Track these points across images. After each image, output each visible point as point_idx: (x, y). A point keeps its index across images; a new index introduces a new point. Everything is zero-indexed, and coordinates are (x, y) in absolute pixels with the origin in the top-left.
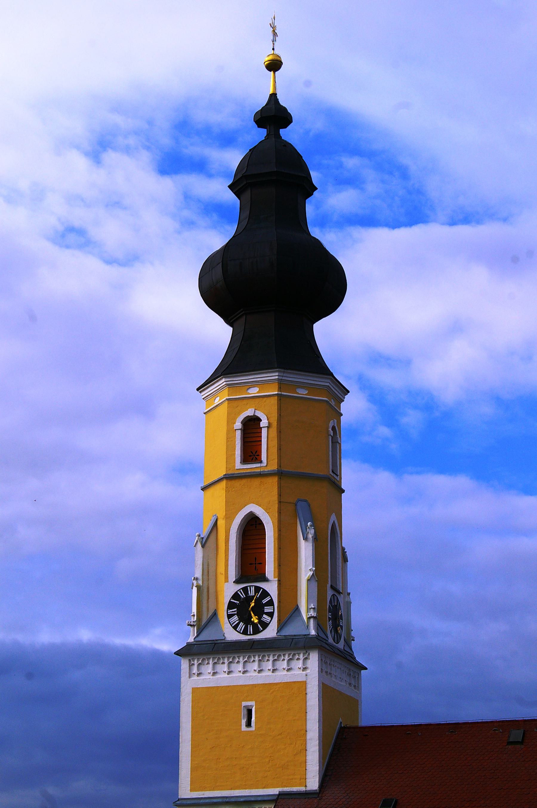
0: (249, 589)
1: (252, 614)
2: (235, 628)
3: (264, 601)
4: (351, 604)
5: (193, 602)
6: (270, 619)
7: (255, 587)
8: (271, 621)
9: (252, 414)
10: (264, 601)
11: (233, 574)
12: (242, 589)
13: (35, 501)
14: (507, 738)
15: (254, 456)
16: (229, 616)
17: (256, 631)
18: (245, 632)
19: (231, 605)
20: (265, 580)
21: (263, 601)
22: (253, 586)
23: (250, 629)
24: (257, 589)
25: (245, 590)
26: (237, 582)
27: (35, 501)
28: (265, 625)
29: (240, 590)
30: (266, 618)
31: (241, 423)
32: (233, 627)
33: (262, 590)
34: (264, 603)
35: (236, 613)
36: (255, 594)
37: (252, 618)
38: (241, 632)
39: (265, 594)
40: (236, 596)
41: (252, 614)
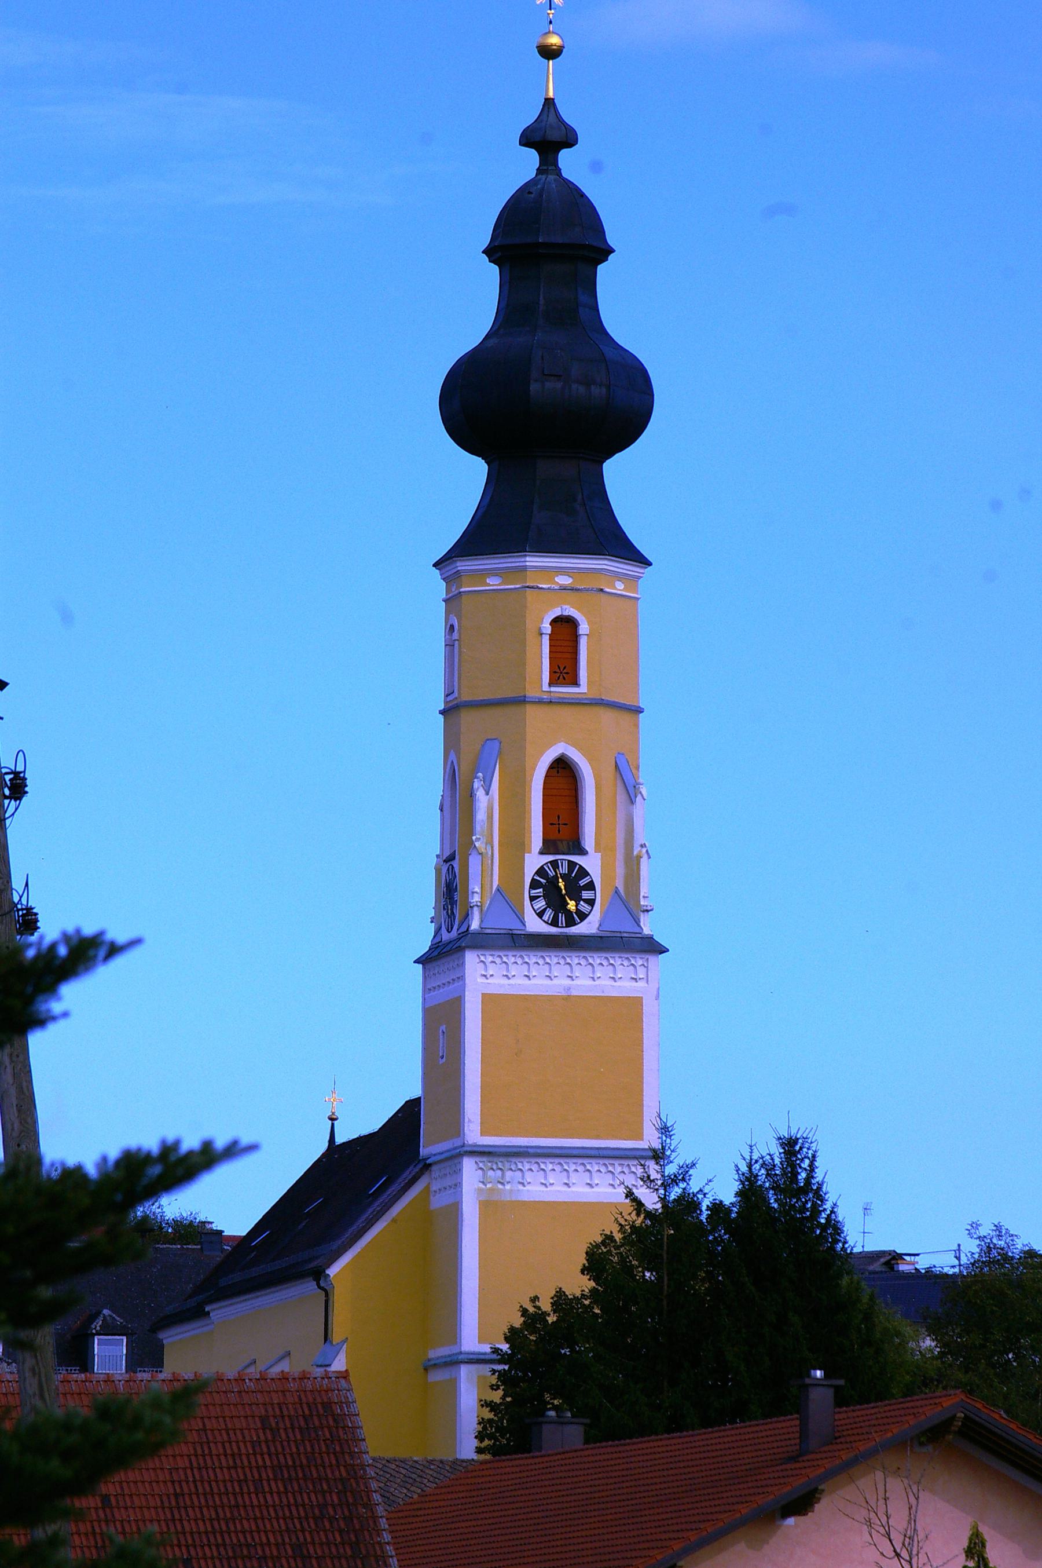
0: (560, 864)
1: (567, 899)
2: (540, 915)
3: (582, 883)
4: (434, 906)
5: (641, 878)
6: (590, 909)
7: (569, 861)
8: (591, 910)
9: (560, 614)
10: (582, 883)
11: (537, 841)
12: (551, 862)
13: (389, 724)
14: (16, 1396)
15: (561, 673)
16: (532, 899)
17: (571, 922)
18: (554, 923)
19: (534, 885)
20: (583, 852)
21: (580, 882)
22: (565, 860)
23: (562, 918)
24: (572, 865)
25: (554, 864)
26: (541, 853)
27: (389, 724)
28: (583, 916)
29: (547, 863)
30: (584, 907)
31: (550, 624)
32: (538, 914)
33: (578, 866)
34: (582, 885)
35: (542, 894)
36: (556, 872)
37: (568, 904)
38: (564, 925)
39: (583, 873)
40: (541, 872)
41: (567, 899)
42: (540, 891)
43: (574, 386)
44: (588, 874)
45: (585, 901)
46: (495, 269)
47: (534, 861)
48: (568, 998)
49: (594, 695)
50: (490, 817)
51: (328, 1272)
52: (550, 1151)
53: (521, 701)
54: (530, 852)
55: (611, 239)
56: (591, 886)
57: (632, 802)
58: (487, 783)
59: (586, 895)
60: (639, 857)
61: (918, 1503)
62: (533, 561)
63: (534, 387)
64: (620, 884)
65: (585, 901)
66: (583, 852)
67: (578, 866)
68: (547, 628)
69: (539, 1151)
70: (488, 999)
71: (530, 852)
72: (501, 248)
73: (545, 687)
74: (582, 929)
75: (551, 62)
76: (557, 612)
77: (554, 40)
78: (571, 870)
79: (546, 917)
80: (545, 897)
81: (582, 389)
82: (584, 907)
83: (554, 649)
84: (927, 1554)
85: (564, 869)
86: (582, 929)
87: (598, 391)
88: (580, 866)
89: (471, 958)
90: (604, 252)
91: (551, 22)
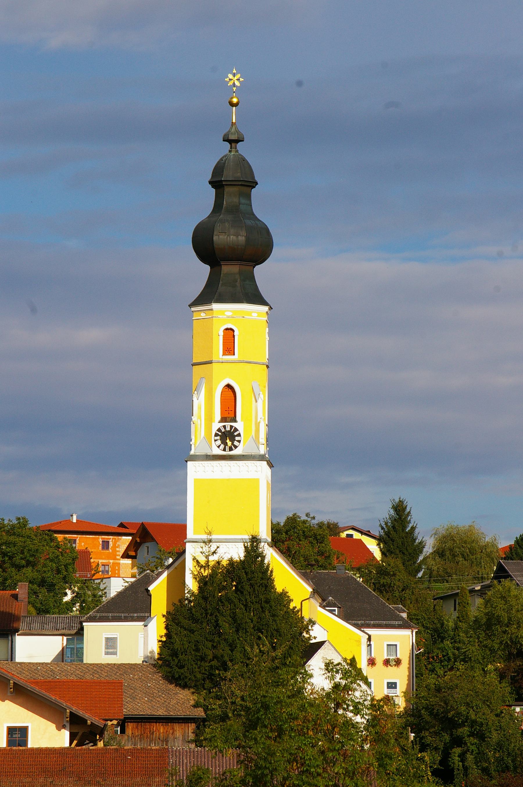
2: (219, 447)
3: (236, 434)
10: (236, 434)
11: (218, 416)
17: (231, 449)
18: (224, 450)
19: (216, 435)
20: (235, 421)
24: (231, 427)
25: (224, 427)
33: (234, 428)
39: (236, 430)
40: (219, 430)
42: (218, 438)
43: (232, 237)
44: (238, 430)
45: (237, 441)
46: (214, 190)
47: (217, 425)
48: (228, 480)
49: (241, 359)
50: (200, 408)
51: (149, 589)
52: (221, 540)
53: (210, 362)
54: (214, 422)
55: (257, 179)
56: (239, 435)
57: (256, 402)
58: (198, 394)
59: (237, 438)
60: (259, 423)
61: (156, 542)
62: (215, 306)
63: (215, 238)
64: (253, 434)
65: (237, 441)
66: (235, 421)
67: (234, 428)
68: (221, 333)
69: (217, 540)
70: (196, 481)
71: (214, 422)
72: (216, 182)
73: (221, 356)
74: (235, 452)
75: (234, 107)
76: (226, 327)
77: (235, 100)
78: (231, 429)
79: (221, 448)
80: (220, 439)
81: (234, 237)
82: (236, 443)
83: (225, 341)
84: (148, 548)
85: (228, 429)
86: (235, 452)
87: (242, 239)
88: (235, 428)
89: (189, 463)
90: (253, 184)
91: (234, 92)
